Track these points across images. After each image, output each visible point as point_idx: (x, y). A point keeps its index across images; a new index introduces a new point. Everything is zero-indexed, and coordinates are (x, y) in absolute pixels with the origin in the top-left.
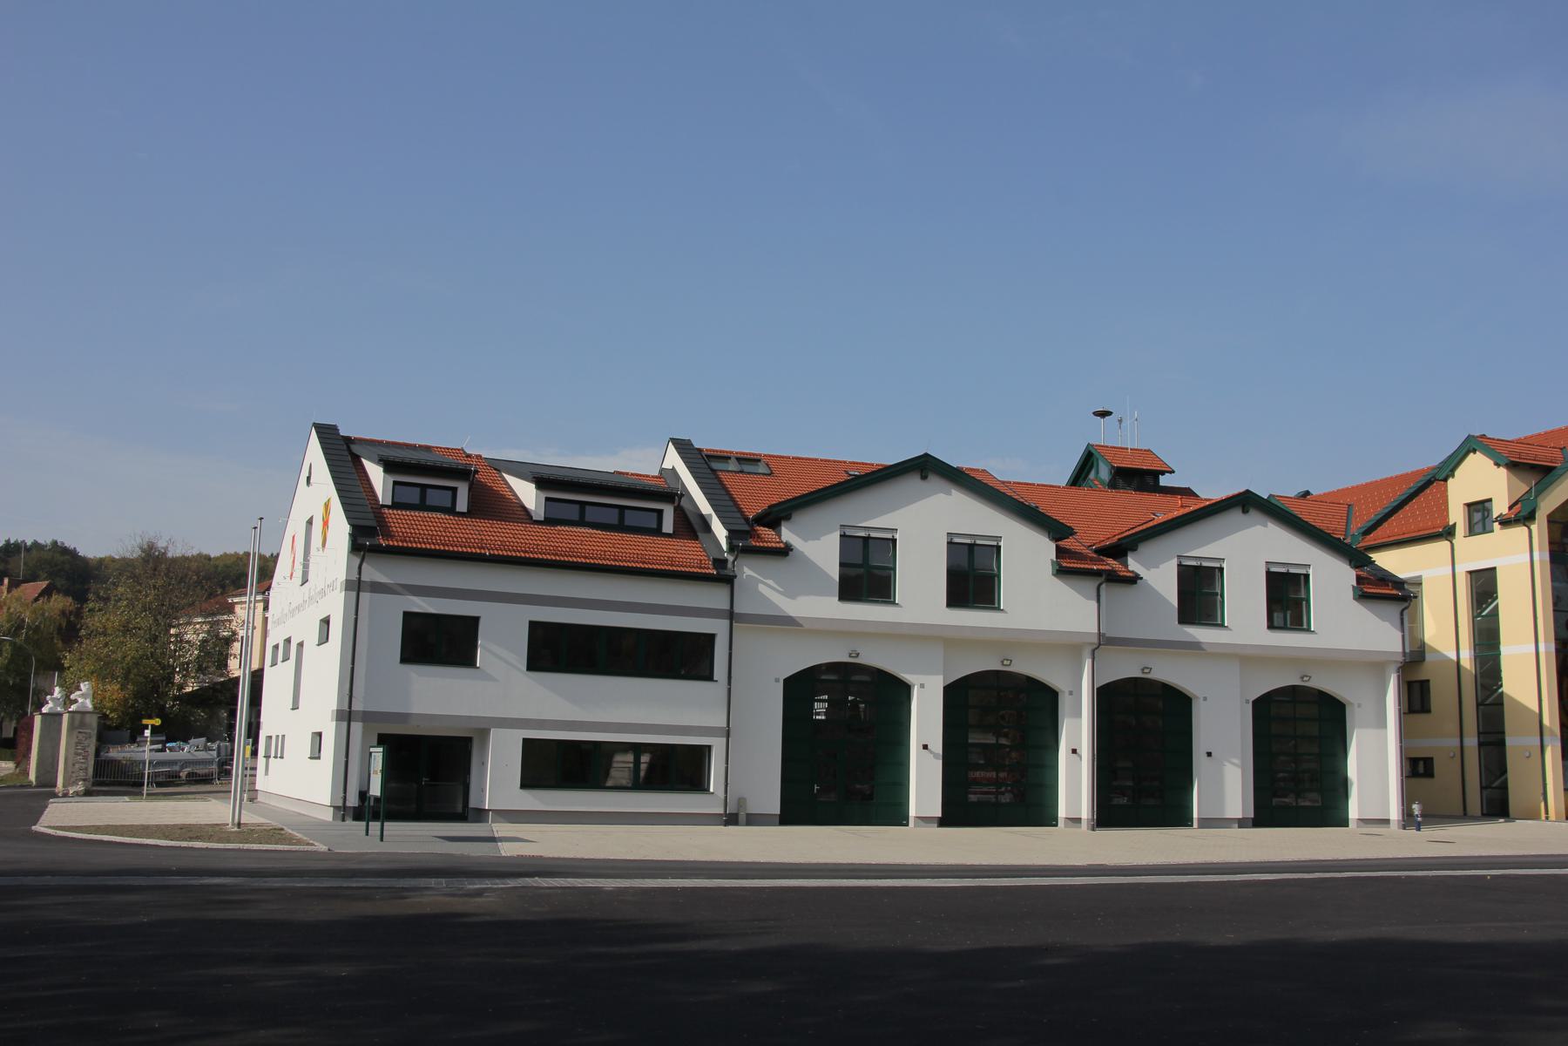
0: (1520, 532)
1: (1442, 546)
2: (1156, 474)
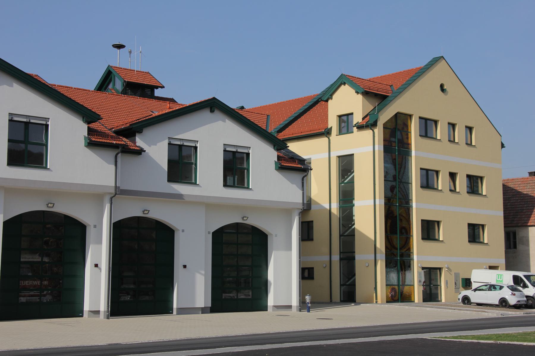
0: (368, 133)
1: (324, 140)
2: (153, 88)
